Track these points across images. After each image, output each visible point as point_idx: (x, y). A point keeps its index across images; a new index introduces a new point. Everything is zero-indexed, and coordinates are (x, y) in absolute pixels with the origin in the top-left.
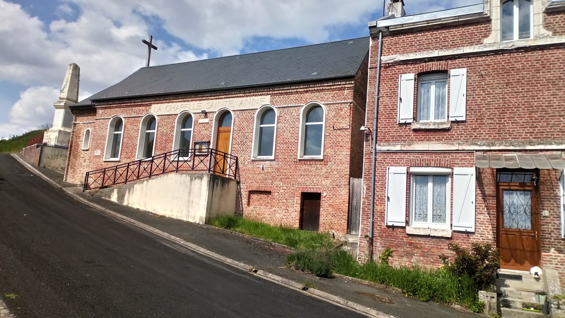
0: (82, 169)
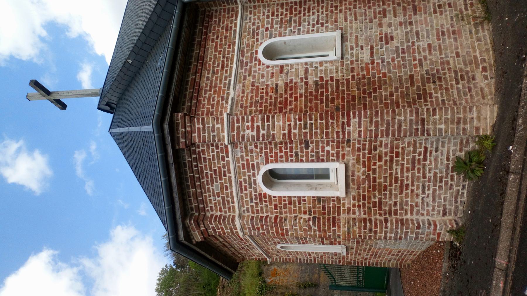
0: (423, 44)
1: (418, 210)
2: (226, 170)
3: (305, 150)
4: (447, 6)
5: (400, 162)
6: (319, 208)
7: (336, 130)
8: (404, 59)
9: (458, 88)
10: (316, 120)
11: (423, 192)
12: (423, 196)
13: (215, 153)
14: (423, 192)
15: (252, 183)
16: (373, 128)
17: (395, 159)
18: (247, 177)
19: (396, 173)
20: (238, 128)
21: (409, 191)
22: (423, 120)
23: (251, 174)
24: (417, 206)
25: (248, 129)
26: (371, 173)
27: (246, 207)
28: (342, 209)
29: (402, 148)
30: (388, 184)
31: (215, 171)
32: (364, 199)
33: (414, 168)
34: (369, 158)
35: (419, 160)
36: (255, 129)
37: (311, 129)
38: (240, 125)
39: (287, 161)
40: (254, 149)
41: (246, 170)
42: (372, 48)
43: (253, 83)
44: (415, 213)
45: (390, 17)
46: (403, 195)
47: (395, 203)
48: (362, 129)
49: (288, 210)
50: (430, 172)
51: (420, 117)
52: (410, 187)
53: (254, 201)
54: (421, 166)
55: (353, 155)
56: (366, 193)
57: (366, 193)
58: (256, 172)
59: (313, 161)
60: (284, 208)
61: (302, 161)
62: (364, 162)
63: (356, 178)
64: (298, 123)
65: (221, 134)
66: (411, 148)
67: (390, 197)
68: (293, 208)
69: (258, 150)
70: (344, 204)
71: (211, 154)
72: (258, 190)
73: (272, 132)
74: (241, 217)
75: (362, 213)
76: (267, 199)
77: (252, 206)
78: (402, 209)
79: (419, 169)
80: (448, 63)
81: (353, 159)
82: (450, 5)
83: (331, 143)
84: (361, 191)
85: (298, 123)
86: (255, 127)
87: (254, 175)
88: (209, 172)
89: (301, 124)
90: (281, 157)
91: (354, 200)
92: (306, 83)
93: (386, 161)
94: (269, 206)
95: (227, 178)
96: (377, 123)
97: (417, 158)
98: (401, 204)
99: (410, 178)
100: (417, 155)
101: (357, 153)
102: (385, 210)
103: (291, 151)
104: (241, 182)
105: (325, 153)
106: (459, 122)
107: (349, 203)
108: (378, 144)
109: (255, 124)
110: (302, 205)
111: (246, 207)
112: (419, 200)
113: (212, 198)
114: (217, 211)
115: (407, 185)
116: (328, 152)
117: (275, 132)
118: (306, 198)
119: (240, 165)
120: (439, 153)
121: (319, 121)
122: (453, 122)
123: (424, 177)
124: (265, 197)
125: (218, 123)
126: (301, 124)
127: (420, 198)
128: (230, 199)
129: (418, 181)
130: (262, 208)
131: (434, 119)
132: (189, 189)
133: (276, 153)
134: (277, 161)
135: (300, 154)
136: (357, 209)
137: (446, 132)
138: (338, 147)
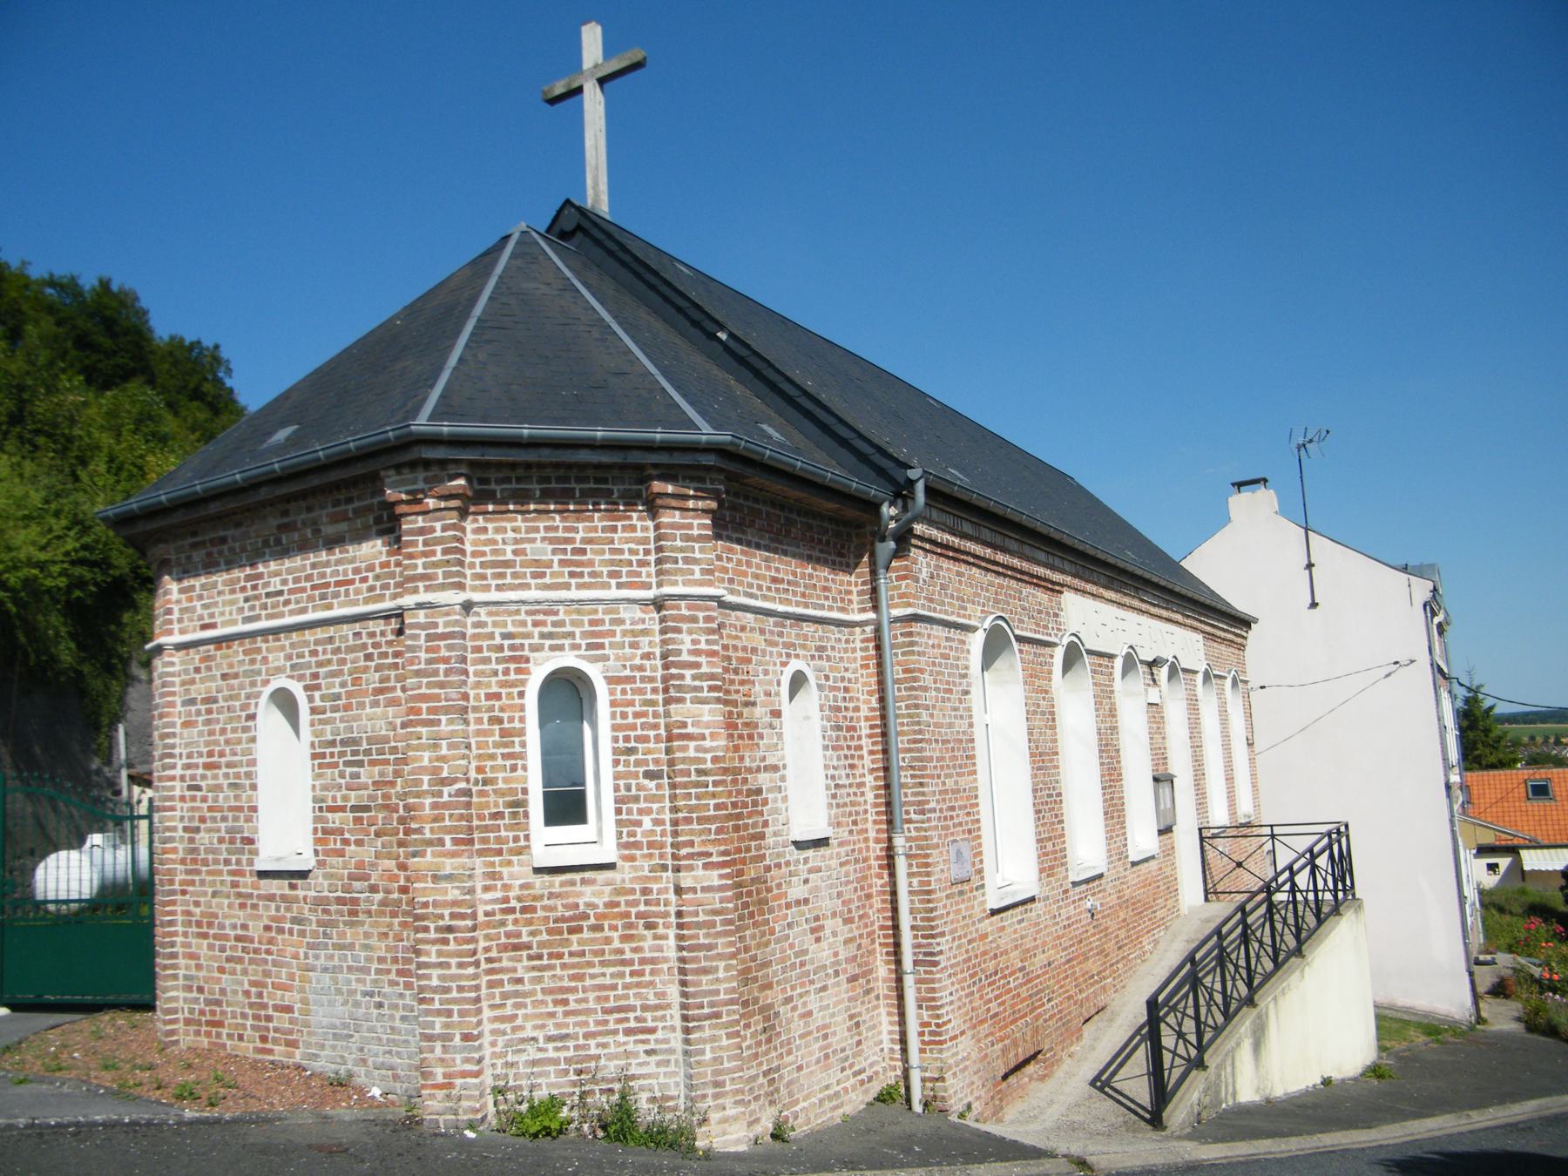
0: (813, 1002)
1: (504, 1033)
2: (586, 579)
3: (641, 770)
4: (857, 1038)
5: (620, 982)
6: (496, 805)
7: (697, 840)
8: (793, 966)
9: (757, 1075)
10: (714, 795)
11: (550, 1039)
12: (541, 1040)
13: (626, 556)
14: (550, 1039)
15: (555, 639)
16: (702, 918)
17: (627, 970)
18: (568, 629)
19: (593, 976)
20: (694, 620)
21: (551, 1009)
22: (717, 1015)
23: (578, 641)
24: (514, 1029)
25: (694, 642)
26: (592, 921)
27: (489, 620)
28: (497, 859)
29: (652, 983)
30: (566, 959)
31: (583, 552)
32: (524, 910)
33: (606, 1011)
34: (627, 915)
35: (627, 1020)
36: (693, 659)
37: (697, 785)
38: (701, 625)
39: (615, 728)
40: (639, 652)
41: (587, 628)
42: (806, 901)
43: (754, 650)
44: (497, 1026)
45: (845, 932)
46: (540, 997)
47: (520, 981)
48: (699, 895)
49: (486, 726)
50: (598, 1045)
51: (724, 1009)
52: (560, 1009)
53: (506, 643)
54: (612, 1026)
55: (633, 880)
56: (540, 913)
57: (540, 913)
58: (582, 652)
59: (617, 789)
60: (490, 719)
61: (616, 763)
62: (618, 904)
63: (578, 888)
64: (708, 756)
65: (680, 579)
66: (652, 1001)
67: (534, 968)
68: (491, 739)
69: (637, 661)
70: (509, 863)
71: (626, 547)
72: (536, 654)
73: (688, 696)
74: (468, 607)
75: (489, 908)
76: (513, 676)
77: (491, 636)
78: (505, 996)
79: (606, 1022)
80: (789, 1053)
81: (623, 881)
82: (859, 1043)
83: (658, 829)
84: (546, 902)
85: (708, 756)
86: (698, 659)
87: (576, 647)
88: (578, 537)
89: (705, 761)
90: (624, 715)
91: (522, 887)
92: (758, 770)
93: (621, 952)
94: (494, 679)
95: (566, 579)
96: (712, 924)
97: (631, 1015)
98: (516, 994)
99: (584, 1006)
100: (638, 1013)
101: (637, 887)
102: (500, 960)
103: (638, 739)
104: (556, 613)
105: (635, 817)
106: (717, 1084)
107: (517, 874)
108: (660, 931)
109: (703, 659)
110: (500, 761)
111: (489, 620)
112: (529, 1033)
113: (511, 535)
114: (474, 543)
115: (565, 1002)
116: (639, 823)
117: (688, 704)
118: (520, 772)
119: (600, 616)
120: (643, 1058)
121: (712, 802)
122: (717, 1073)
123: (587, 1036)
124: (518, 671)
125: (704, 572)
126: (705, 761)
127: (534, 1034)
128: (508, 580)
129: (576, 1024)
130: (487, 660)
131: (720, 1037)
132: (539, 482)
133: (631, 703)
134: (613, 704)
135: (632, 758)
136: (499, 894)
137: (698, 1063)
138: (651, 845)
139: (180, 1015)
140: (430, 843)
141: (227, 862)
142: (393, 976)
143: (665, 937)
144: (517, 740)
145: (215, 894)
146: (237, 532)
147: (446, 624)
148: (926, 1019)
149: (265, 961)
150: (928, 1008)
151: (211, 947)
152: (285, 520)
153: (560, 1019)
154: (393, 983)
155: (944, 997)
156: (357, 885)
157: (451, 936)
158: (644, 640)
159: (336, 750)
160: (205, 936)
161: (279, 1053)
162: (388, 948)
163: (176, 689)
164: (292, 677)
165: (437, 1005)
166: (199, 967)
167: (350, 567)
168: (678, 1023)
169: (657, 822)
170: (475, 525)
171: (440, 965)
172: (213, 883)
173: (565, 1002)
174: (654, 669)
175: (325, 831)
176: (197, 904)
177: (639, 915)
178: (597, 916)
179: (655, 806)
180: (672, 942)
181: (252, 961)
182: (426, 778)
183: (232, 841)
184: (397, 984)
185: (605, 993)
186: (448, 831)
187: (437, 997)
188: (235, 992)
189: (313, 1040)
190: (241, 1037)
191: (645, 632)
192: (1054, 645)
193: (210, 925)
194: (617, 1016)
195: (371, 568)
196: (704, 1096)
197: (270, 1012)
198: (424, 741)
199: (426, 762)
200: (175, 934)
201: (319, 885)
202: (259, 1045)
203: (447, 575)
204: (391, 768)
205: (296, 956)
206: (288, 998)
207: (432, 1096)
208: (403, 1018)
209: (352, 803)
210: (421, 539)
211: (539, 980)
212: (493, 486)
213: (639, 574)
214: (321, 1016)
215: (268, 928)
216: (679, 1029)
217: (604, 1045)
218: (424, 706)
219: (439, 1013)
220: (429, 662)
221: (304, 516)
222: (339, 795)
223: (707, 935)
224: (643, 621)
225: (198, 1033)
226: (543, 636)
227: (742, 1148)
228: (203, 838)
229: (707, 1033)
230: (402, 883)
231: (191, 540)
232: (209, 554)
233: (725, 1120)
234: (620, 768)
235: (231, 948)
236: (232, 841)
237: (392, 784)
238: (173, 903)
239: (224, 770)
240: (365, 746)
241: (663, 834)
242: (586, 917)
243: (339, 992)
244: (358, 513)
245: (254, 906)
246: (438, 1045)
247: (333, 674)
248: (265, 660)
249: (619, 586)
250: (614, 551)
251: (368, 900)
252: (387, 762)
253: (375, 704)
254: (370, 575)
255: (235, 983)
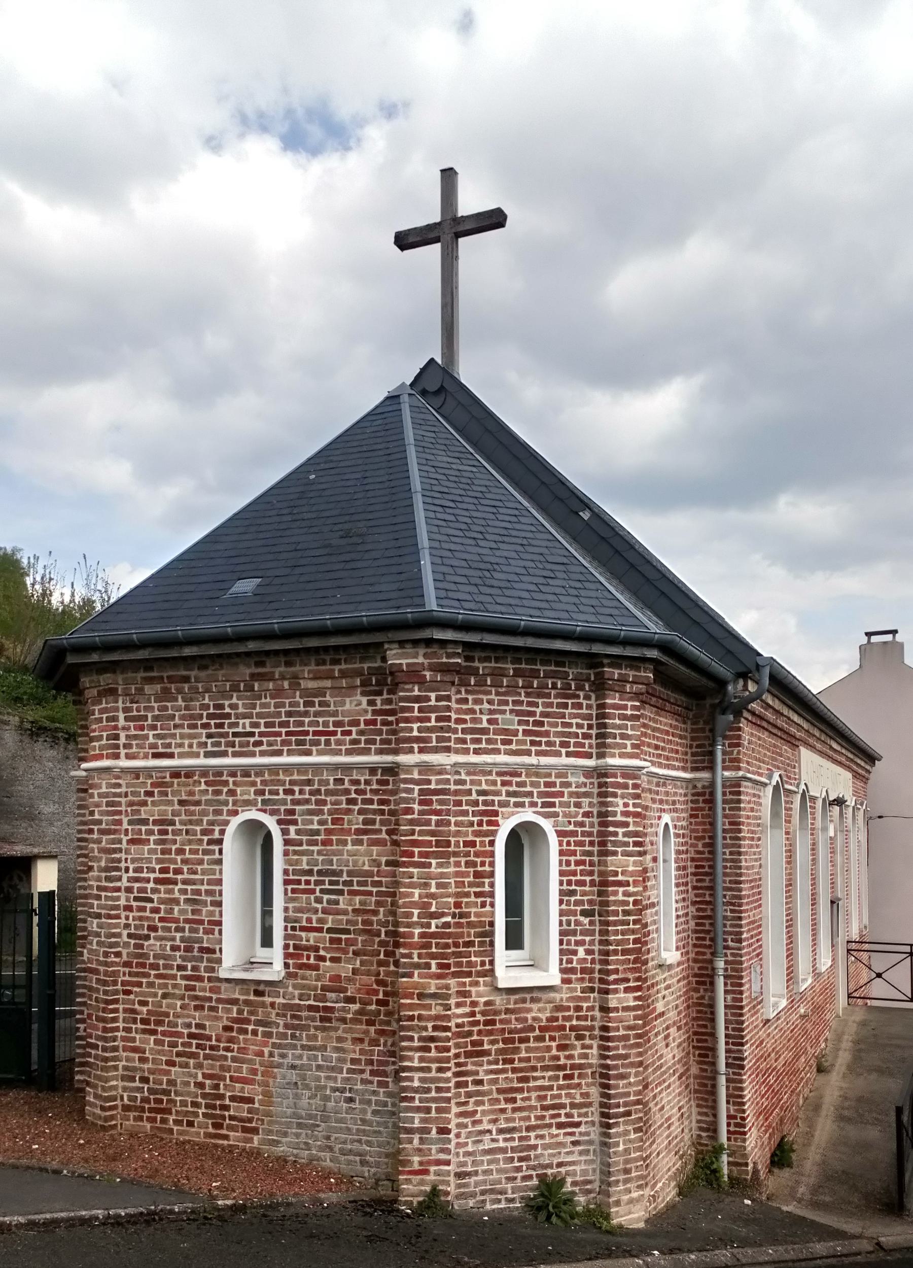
1: (466, 1126)
2: (543, 747)
3: (579, 908)
5: (555, 1084)
6: (469, 935)
11: (501, 1131)
12: (494, 1132)
13: (574, 729)
14: (501, 1131)
15: (519, 798)
17: (561, 1074)
18: (528, 789)
20: (626, 786)
21: (503, 1105)
23: (535, 799)
24: (474, 1123)
25: (626, 805)
26: (537, 1032)
28: (467, 980)
29: (579, 1085)
30: (516, 1064)
32: (487, 1023)
33: (544, 1108)
35: (559, 1115)
36: (624, 819)
38: (631, 791)
39: (562, 873)
40: (581, 811)
41: (542, 789)
44: (461, 1120)
46: (495, 1095)
47: (480, 1082)
50: (537, 1137)
53: (481, 798)
54: (547, 1121)
55: (568, 999)
59: (561, 924)
60: (467, 863)
62: (557, 1019)
63: (527, 1005)
64: (631, 899)
65: (617, 751)
66: (578, 1100)
71: (574, 721)
72: (504, 809)
73: (619, 850)
75: (460, 1021)
76: (485, 827)
77: (469, 793)
78: (469, 1095)
83: (589, 957)
84: (503, 1016)
85: (631, 899)
87: (533, 804)
90: (568, 863)
91: (487, 1003)
93: (557, 1058)
94: (470, 829)
97: (563, 1112)
98: (478, 1093)
99: (527, 1103)
103: (578, 883)
105: (573, 947)
108: (587, 1042)
109: (630, 820)
110: (473, 899)
111: (468, 778)
112: (485, 1126)
113: (486, 706)
115: (514, 1100)
116: (575, 953)
118: (488, 908)
119: (553, 779)
121: (632, 937)
123: (528, 1129)
124: (490, 823)
125: (634, 746)
127: (489, 1127)
128: (484, 745)
129: (521, 1119)
130: (465, 813)
132: (512, 663)
133: (574, 853)
134: (561, 853)
135: (573, 899)
136: (468, 1010)
137: (615, 1153)
138: (583, 971)
139: (118, 1102)
140: (417, 966)
141: (180, 968)
142: (366, 1076)
143: (590, 1047)
144: (487, 881)
145: (165, 996)
146: (203, 674)
147: (438, 782)
148: (732, 1112)
149: (226, 1058)
150: (734, 1104)
151: (157, 1042)
152: (260, 670)
153: (509, 1114)
154: (364, 1082)
155: (748, 1094)
156: (332, 995)
157: (432, 1045)
158: (585, 801)
159: (312, 879)
160: (153, 1032)
161: (235, 1137)
162: (362, 1052)
163: (123, 808)
164: (265, 811)
165: (417, 1103)
166: (143, 1060)
167: (331, 719)
168: (596, 1118)
169: (588, 952)
170: (459, 696)
171: (421, 1069)
172: (161, 986)
173: (514, 1100)
174: (592, 825)
175: (296, 947)
176: (143, 1003)
177: (572, 1028)
178: (541, 1029)
179: (588, 939)
180: (595, 1051)
181: (206, 1057)
182: (416, 912)
183: (188, 949)
184: (371, 1082)
185: (543, 1093)
186: (433, 956)
187: (417, 1096)
188: (187, 1084)
189: (276, 1128)
190: (190, 1124)
191: (586, 795)
192: (765, 785)
193: (159, 1023)
194: (552, 1112)
195: (356, 723)
196: (618, 1181)
197: (227, 1102)
198: (415, 880)
199: (416, 898)
200: (117, 1029)
201: (292, 994)
202: (211, 1130)
203: (439, 740)
204: (374, 899)
205: (260, 1054)
206: (248, 1090)
207: (408, 1181)
208: (375, 1113)
209: (329, 925)
210: (416, 706)
211: (495, 1081)
212: (476, 664)
213: (583, 745)
214: (283, 1107)
215: (227, 1029)
216: (597, 1124)
217: (542, 1137)
218: (416, 850)
219: (418, 1109)
220: (421, 813)
221: (282, 669)
222: (314, 917)
223: (624, 1047)
224: (585, 785)
225: (141, 1119)
226: (509, 794)
227: (641, 1225)
228: (153, 945)
229: (621, 1129)
230: (381, 996)
231: (142, 674)
232: (166, 691)
233: (631, 1201)
234: (564, 907)
235: (183, 1044)
236: (188, 949)
237: (375, 913)
238: (116, 1001)
239: (180, 886)
240: (345, 877)
241: (593, 961)
242: (532, 1029)
243: (307, 1087)
244: (344, 674)
245: (212, 1009)
246: (416, 1138)
247: (311, 812)
248: (232, 793)
249: (568, 754)
250: (565, 725)
251: (343, 1009)
252: (370, 893)
253: (359, 842)
254: (354, 729)
255: (186, 1078)
